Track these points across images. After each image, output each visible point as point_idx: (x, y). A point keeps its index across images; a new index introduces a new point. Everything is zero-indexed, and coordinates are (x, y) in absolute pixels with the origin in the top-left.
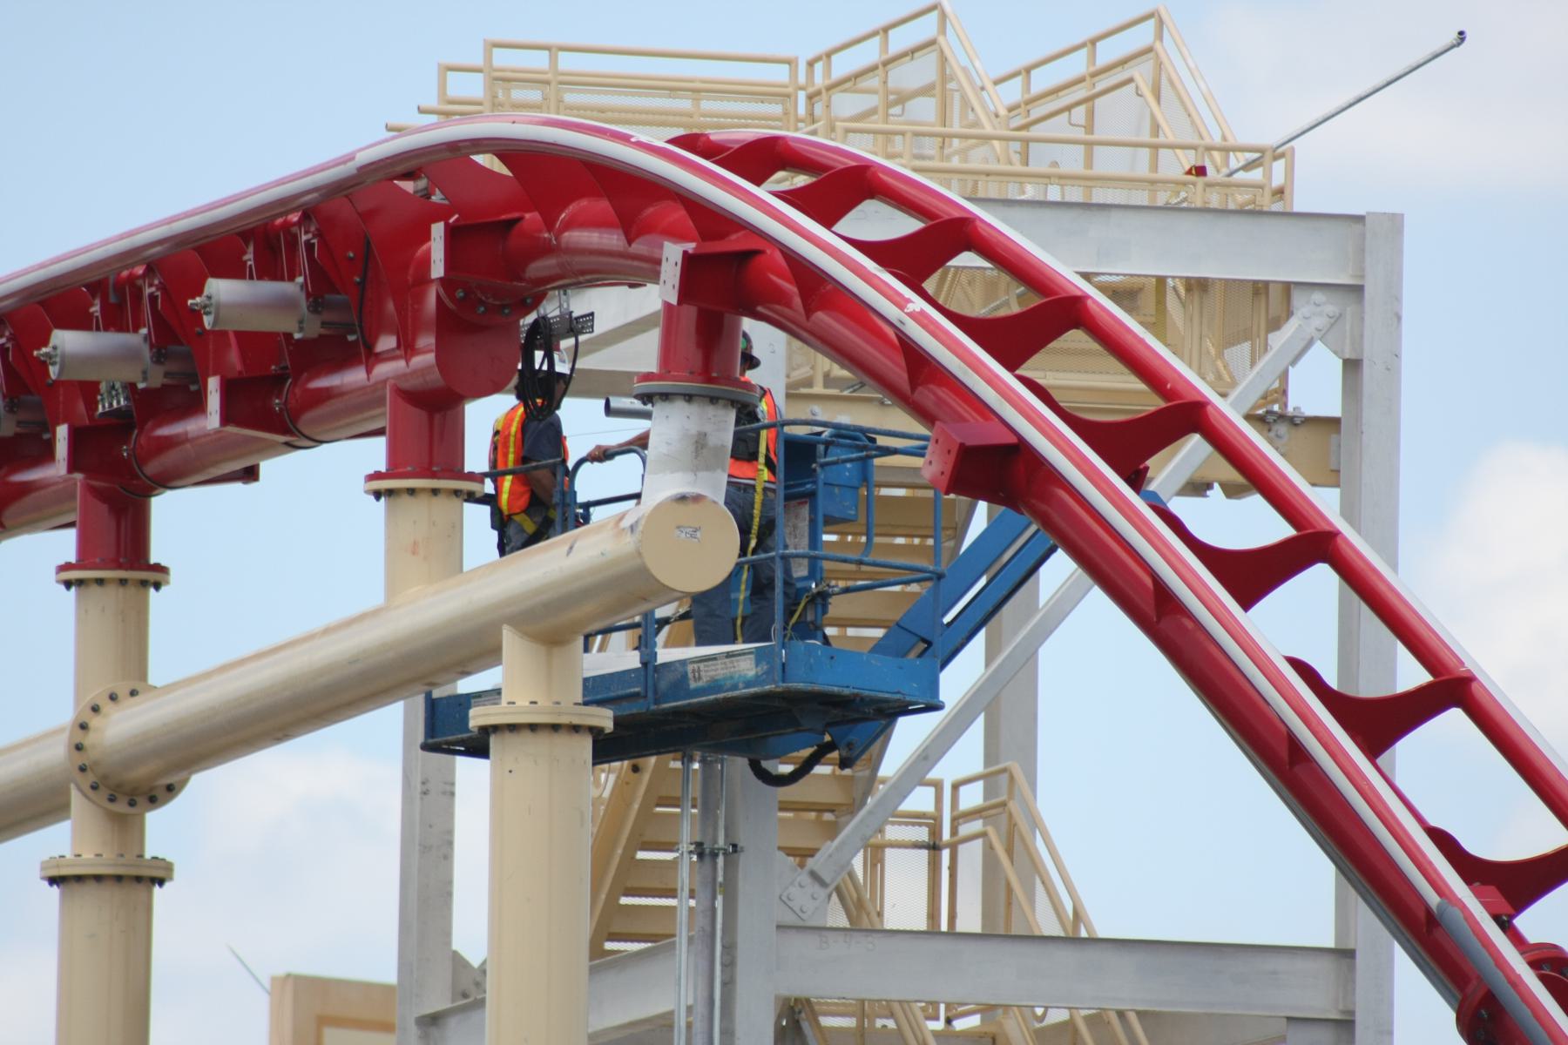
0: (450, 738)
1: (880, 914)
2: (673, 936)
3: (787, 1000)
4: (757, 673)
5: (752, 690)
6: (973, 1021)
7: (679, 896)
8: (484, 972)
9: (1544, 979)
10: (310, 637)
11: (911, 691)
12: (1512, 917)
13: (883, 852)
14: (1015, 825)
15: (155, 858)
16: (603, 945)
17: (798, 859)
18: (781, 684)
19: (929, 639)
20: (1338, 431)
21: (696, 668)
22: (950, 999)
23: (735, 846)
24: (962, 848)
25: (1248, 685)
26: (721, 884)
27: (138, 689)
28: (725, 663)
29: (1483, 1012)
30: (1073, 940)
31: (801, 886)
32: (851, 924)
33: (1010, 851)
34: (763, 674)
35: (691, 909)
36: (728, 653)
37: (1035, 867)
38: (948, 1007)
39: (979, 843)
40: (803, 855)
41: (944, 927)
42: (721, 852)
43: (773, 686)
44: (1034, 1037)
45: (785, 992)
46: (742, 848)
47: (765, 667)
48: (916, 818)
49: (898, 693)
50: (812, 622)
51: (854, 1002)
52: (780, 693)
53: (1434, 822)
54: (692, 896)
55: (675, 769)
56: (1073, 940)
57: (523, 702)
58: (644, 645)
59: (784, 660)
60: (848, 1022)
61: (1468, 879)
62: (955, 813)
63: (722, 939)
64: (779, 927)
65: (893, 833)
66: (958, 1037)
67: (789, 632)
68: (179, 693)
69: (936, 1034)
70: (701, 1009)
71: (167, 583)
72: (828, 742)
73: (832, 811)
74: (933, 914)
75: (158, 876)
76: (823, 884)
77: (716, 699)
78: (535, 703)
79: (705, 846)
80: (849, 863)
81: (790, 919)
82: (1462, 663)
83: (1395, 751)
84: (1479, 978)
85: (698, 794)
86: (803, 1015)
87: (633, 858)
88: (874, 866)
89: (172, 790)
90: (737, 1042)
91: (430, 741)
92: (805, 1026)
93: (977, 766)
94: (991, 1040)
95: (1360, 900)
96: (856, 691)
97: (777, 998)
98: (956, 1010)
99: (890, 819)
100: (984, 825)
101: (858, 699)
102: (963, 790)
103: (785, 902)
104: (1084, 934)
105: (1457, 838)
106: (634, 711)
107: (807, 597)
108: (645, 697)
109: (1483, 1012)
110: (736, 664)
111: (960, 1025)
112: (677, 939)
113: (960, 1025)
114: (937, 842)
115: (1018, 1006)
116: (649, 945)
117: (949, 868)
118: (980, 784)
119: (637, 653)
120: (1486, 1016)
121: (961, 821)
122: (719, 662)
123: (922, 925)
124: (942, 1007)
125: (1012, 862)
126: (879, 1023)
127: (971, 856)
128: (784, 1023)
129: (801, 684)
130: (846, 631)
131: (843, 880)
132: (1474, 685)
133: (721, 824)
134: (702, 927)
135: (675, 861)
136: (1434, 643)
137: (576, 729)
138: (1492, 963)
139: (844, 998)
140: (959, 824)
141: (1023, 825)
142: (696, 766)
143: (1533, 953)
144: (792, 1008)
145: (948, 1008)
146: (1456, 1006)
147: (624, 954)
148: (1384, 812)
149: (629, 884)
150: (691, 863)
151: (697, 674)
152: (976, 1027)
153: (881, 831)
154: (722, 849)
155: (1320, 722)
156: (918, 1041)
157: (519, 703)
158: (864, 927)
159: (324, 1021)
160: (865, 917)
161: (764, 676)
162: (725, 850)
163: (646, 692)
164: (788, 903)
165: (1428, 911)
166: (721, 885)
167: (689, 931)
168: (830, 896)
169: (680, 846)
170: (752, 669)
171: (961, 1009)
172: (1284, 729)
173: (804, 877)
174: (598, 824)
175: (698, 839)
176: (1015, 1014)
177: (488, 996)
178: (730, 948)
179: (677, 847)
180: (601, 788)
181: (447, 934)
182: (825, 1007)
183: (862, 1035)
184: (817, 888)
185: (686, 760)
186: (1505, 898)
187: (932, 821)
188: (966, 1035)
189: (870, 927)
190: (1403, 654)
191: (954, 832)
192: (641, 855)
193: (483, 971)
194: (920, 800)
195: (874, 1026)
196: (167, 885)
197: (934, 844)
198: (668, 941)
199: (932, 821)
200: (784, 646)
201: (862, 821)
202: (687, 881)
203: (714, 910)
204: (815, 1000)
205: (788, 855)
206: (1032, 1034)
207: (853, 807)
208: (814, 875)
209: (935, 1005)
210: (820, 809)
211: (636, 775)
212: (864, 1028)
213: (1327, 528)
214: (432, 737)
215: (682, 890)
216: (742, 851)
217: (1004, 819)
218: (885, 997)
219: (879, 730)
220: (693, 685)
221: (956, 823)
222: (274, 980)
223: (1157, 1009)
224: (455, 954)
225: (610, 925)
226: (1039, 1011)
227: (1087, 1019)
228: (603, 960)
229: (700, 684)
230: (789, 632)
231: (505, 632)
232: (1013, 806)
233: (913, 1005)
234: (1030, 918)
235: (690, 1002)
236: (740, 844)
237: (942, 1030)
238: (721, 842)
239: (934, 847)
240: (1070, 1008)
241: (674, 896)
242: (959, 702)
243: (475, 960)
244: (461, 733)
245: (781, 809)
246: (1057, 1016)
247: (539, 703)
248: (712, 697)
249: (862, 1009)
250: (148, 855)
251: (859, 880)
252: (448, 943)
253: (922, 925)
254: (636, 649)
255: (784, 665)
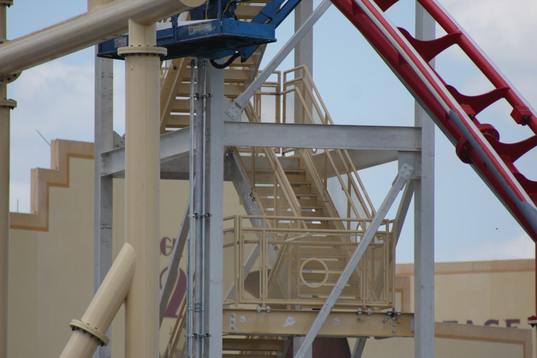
0: (107, 52)
1: (260, 118)
2: (189, 125)
3: (228, 147)
4: (212, 29)
5: (211, 35)
6: (292, 154)
7: (191, 112)
8: (124, 138)
9: (486, 137)
10: (62, 23)
11: (266, 36)
12: (475, 115)
13: (260, 96)
14: (305, 86)
15: (10, 99)
16: (165, 129)
17: (231, 99)
18: (220, 33)
19: (271, 17)
21: (191, 28)
22: (284, 146)
23: (209, 95)
24: (287, 95)
25: (387, 39)
26: (205, 108)
27: (3, 41)
28: (201, 26)
29: (465, 148)
30: (325, 126)
31: (233, 108)
32: (250, 121)
33: (304, 96)
34: (214, 30)
35: (195, 116)
36: (202, 22)
37: (312, 101)
38: (283, 149)
39: (293, 93)
40: (233, 97)
41: (281, 122)
42: (205, 97)
43: (218, 34)
44: (312, 158)
45: (227, 144)
46: (212, 95)
47: (215, 27)
48: (271, 84)
49: (261, 36)
50: (231, 12)
51: (251, 148)
52: (220, 36)
53: (448, 83)
54: (195, 112)
55: (189, 68)
56: (325, 126)
57: (136, 46)
58: (174, 20)
59: (221, 25)
60: (249, 154)
61: (460, 102)
62: (285, 83)
63: (206, 126)
64: (225, 122)
65: (264, 89)
66: (287, 159)
67: (223, 15)
68: (18, 42)
69: (279, 158)
70: (199, 150)
71: (12, 4)
72: (237, 53)
73: (243, 82)
74: (278, 118)
75: (12, 105)
76: (240, 107)
77: (198, 39)
78: (140, 46)
79: (199, 95)
80: (249, 100)
81: (229, 119)
82: (458, 28)
83: (435, 59)
84: (464, 137)
85: (197, 77)
86: (234, 152)
87: (175, 99)
88: (257, 101)
89: (16, 76)
91: (100, 53)
92: (234, 156)
93: (292, 66)
94: (298, 160)
95: (423, 110)
96: (246, 35)
97: (225, 146)
98: (286, 150)
99: (263, 85)
100: (295, 87)
101: (247, 38)
102: (287, 74)
103: (227, 114)
104: (329, 123)
105: (409, 33)
106: (170, 43)
107: (229, 3)
108: (174, 38)
109: (465, 148)
110: (205, 27)
111: (287, 155)
112: (190, 126)
113: (287, 155)
114: (279, 93)
115: (307, 148)
116: (181, 129)
117: (283, 101)
118: (293, 73)
119: (171, 23)
120: (466, 149)
121: (287, 85)
122: (199, 26)
123: (273, 121)
124: (281, 149)
125: (305, 99)
126: (260, 154)
127: (291, 97)
128: (227, 155)
129: (228, 33)
130: (247, 20)
131: (247, 106)
132: (462, 36)
133: (205, 87)
134: (199, 123)
135: (189, 100)
136: (448, 22)
137: (154, 55)
138: (468, 131)
139: (247, 146)
140: (286, 86)
141: (308, 86)
142: (196, 67)
143: (482, 127)
144: (230, 150)
145: (283, 150)
146: (456, 145)
147: (172, 132)
148: (432, 81)
149: (173, 108)
150: (195, 101)
151: (192, 30)
152: (293, 155)
153: (260, 89)
154: (205, 96)
155: (421, 65)
156: (273, 161)
157: (134, 46)
158: (254, 122)
159: (69, 155)
160: (254, 118)
161: (215, 31)
162: (206, 96)
163: (174, 36)
164: (232, 118)
165: (446, 113)
166: (205, 108)
167: (194, 124)
168: (242, 112)
169: (191, 95)
170: (210, 28)
171: (287, 150)
172: (397, 52)
173: (233, 105)
174: (162, 88)
175: (197, 92)
176: (306, 151)
177: (126, 146)
178: (208, 130)
179: (190, 95)
180: (163, 75)
181: (111, 125)
182: (241, 149)
183: (254, 159)
184: (238, 109)
185: (192, 65)
186: (473, 109)
187: (277, 86)
188: (289, 158)
189: (256, 122)
190: (438, 26)
191: (285, 89)
192: (177, 98)
193: (124, 137)
194: (273, 78)
195: (258, 156)
196: (15, 109)
197: (278, 93)
198: (187, 127)
199: (277, 86)
200: (221, 20)
201: (253, 85)
202: (193, 107)
203: (202, 116)
204: (238, 147)
205: (228, 97)
206: (312, 157)
207: (250, 81)
208: (237, 104)
209: (279, 148)
210: (239, 81)
212: (254, 156)
213: (506, 86)
214: (101, 52)
215: (192, 110)
217: (302, 84)
218: (261, 146)
219: (255, 49)
220: (190, 34)
221: (285, 86)
222: (52, 141)
223: (354, 149)
224: (114, 132)
225: (167, 122)
226: (314, 150)
227: (330, 152)
228: (165, 134)
229: (193, 33)
230: (223, 15)
231: (129, 21)
232: (305, 80)
233: (271, 148)
234: (311, 118)
235: (195, 148)
237: (281, 157)
238: (205, 93)
239: (278, 94)
240: (324, 149)
241: (189, 112)
242: (286, 45)
243: (121, 135)
244: (111, 51)
245: (225, 82)
246: (320, 151)
247: (142, 46)
248: (197, 38)
249: (254, 150)
250: (8, 98)
251: (252, 106)
252: (112, 128)
253: (273, 121)
254: (170, 21)
255: (221, 26)
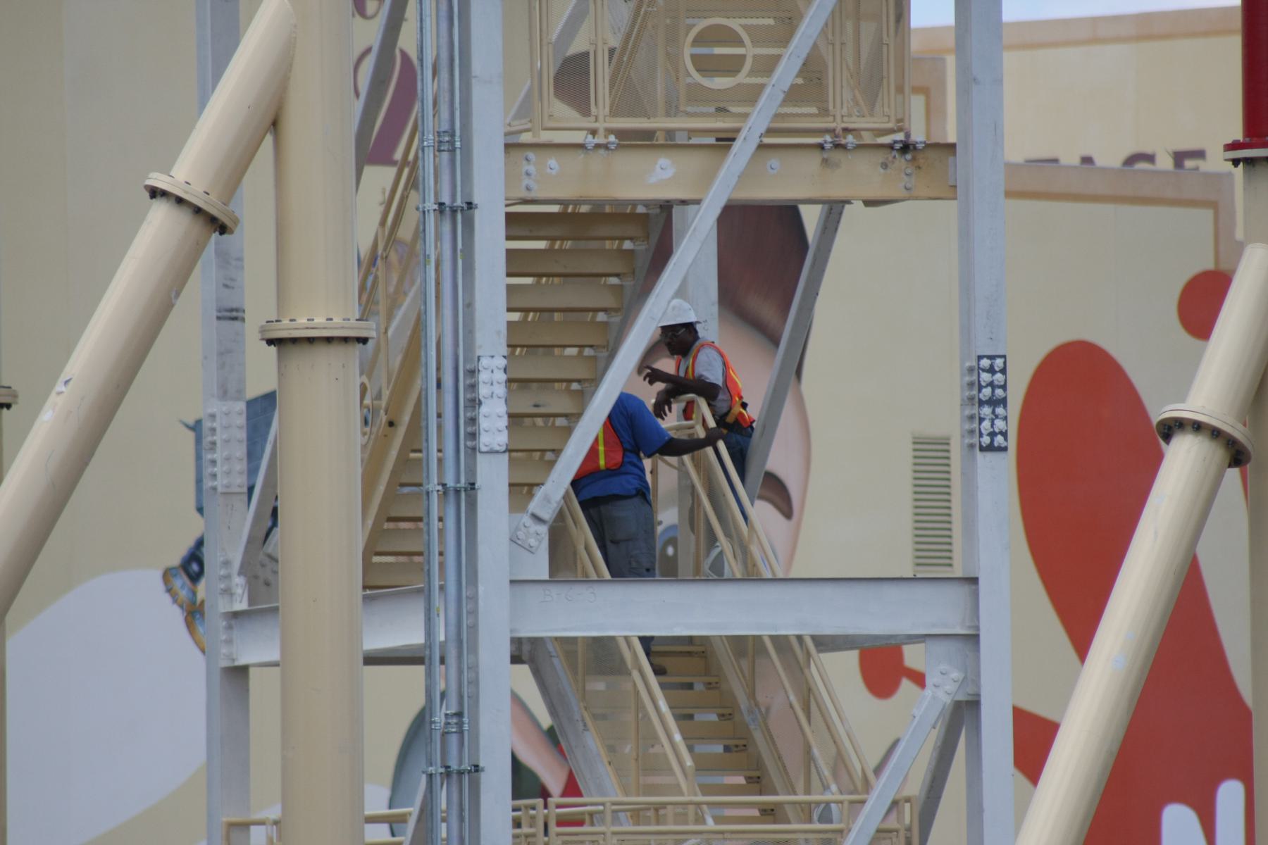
20: (954, 154)
64: (512, 582)
90: (482, 842)
162: (462, 207)
196: (14, 407)
211: (393, 428)
216: (476, 208)
236: (481, 764)
